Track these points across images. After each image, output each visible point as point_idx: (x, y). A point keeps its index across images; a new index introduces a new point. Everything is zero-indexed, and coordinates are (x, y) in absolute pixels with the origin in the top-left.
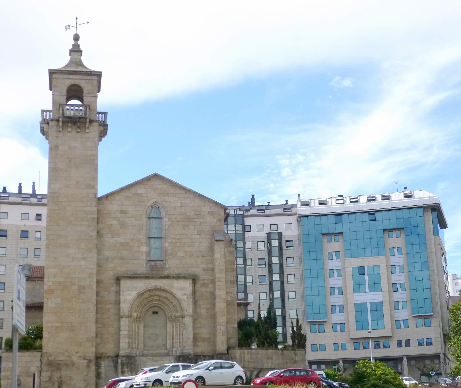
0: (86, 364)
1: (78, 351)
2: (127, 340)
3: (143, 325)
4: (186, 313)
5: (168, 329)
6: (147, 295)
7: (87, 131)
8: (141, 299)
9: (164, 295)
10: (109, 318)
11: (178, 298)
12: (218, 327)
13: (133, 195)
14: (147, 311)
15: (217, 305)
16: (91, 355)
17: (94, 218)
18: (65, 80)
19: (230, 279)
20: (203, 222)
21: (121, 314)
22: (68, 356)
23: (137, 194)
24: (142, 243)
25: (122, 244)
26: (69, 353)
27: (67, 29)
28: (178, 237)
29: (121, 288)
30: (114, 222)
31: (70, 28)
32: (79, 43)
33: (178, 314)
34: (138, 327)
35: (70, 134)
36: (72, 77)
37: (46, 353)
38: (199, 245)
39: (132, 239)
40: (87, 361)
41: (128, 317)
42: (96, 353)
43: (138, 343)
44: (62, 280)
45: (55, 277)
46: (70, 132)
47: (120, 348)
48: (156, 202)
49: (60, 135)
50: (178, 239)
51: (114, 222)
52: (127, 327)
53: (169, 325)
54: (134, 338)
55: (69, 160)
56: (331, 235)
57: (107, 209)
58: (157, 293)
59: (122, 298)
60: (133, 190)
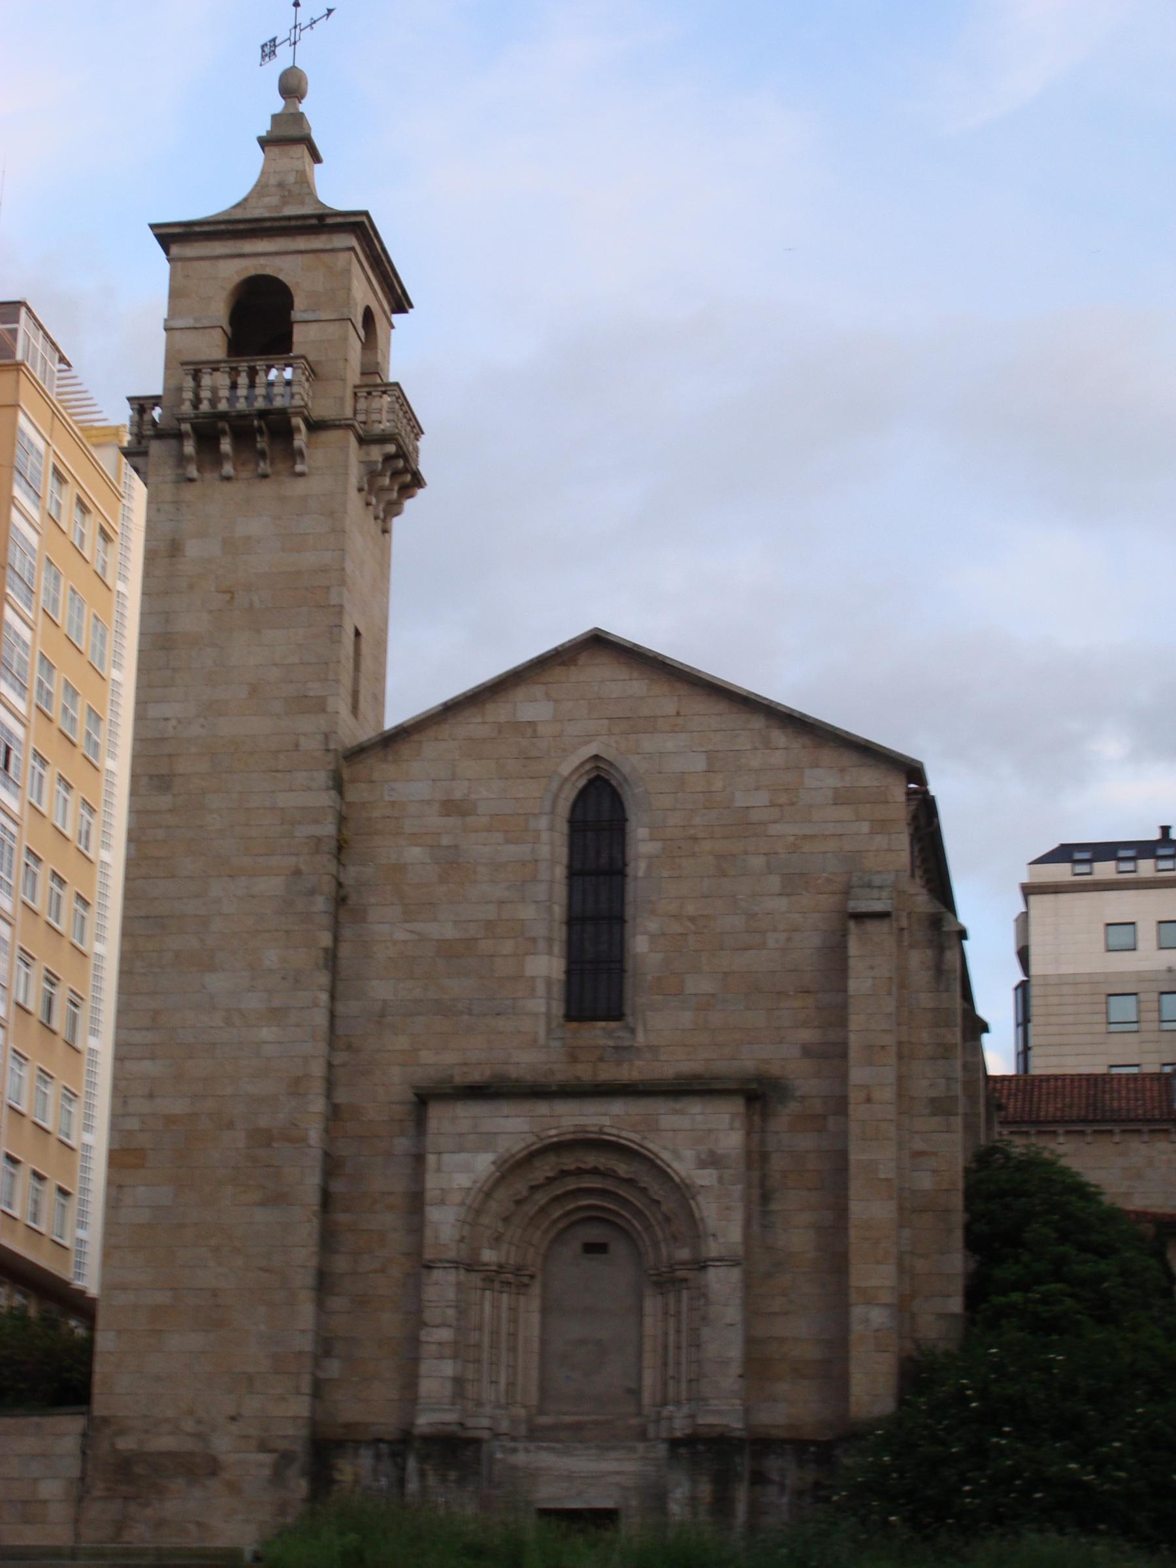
0: (267, 1472)
1: (239, 1415)
2: (448, 1368)
3: (536, 1304)
4: (713, 1249)
5: (648, 1321)
6: (544, 1169)
7: (299, 468)
8: (520, 1187)
9: (623, 1169)
10: (383, 1270)
11: (677, 1179)
12: (857, 1312)
13: (500, 732)
14: (559, 1238)
15: (856, 1208)
16: (290, 1432)
17: (319, 840)
18: (222, 264)
19: (933, 1093)
20: (805, 837)
21: (428, 1255)
22: (199, 1436)
23: (517, 727)
24: (534, 940)
25: (449, 950)
26: (199, 1422)
27: (267, 59)
28: (690, 909)
29: (430, 1140)
30: (415, 853)
31: (278, 50)
32: (303, 107)
33: (684, 1254)
34: (513, 1310)
35: (227, 487)
36: (248, 246)
37: (105, 1421)
38: (789, 939)
39: (489, 925)
40: (275, 1455)
41: (456, 1264)
42: (313, 1423)
43: (511, 1384)
44: (178, 1107)
45: (151, 1096)
46: (228, 479)
47: (421, 1401)
48: (596, 757)
49: (189, 493)
50: (692, 919)
51: (415, 853)
52: (451, 1312)
53: (652, 1305)
54: (485, 1356)
55: (227, 597)
56: (47, 339)
57: (387, 798)
58: (592, 1160)
59: (432, 1182)
60: (498, 712)
